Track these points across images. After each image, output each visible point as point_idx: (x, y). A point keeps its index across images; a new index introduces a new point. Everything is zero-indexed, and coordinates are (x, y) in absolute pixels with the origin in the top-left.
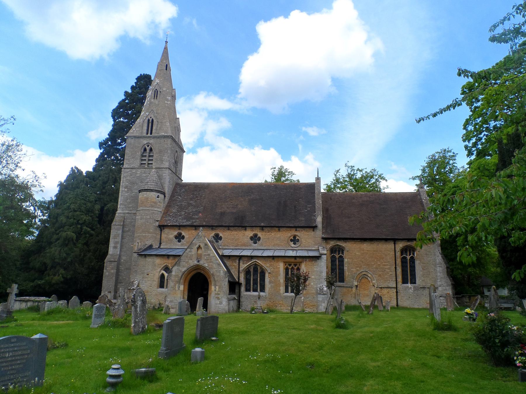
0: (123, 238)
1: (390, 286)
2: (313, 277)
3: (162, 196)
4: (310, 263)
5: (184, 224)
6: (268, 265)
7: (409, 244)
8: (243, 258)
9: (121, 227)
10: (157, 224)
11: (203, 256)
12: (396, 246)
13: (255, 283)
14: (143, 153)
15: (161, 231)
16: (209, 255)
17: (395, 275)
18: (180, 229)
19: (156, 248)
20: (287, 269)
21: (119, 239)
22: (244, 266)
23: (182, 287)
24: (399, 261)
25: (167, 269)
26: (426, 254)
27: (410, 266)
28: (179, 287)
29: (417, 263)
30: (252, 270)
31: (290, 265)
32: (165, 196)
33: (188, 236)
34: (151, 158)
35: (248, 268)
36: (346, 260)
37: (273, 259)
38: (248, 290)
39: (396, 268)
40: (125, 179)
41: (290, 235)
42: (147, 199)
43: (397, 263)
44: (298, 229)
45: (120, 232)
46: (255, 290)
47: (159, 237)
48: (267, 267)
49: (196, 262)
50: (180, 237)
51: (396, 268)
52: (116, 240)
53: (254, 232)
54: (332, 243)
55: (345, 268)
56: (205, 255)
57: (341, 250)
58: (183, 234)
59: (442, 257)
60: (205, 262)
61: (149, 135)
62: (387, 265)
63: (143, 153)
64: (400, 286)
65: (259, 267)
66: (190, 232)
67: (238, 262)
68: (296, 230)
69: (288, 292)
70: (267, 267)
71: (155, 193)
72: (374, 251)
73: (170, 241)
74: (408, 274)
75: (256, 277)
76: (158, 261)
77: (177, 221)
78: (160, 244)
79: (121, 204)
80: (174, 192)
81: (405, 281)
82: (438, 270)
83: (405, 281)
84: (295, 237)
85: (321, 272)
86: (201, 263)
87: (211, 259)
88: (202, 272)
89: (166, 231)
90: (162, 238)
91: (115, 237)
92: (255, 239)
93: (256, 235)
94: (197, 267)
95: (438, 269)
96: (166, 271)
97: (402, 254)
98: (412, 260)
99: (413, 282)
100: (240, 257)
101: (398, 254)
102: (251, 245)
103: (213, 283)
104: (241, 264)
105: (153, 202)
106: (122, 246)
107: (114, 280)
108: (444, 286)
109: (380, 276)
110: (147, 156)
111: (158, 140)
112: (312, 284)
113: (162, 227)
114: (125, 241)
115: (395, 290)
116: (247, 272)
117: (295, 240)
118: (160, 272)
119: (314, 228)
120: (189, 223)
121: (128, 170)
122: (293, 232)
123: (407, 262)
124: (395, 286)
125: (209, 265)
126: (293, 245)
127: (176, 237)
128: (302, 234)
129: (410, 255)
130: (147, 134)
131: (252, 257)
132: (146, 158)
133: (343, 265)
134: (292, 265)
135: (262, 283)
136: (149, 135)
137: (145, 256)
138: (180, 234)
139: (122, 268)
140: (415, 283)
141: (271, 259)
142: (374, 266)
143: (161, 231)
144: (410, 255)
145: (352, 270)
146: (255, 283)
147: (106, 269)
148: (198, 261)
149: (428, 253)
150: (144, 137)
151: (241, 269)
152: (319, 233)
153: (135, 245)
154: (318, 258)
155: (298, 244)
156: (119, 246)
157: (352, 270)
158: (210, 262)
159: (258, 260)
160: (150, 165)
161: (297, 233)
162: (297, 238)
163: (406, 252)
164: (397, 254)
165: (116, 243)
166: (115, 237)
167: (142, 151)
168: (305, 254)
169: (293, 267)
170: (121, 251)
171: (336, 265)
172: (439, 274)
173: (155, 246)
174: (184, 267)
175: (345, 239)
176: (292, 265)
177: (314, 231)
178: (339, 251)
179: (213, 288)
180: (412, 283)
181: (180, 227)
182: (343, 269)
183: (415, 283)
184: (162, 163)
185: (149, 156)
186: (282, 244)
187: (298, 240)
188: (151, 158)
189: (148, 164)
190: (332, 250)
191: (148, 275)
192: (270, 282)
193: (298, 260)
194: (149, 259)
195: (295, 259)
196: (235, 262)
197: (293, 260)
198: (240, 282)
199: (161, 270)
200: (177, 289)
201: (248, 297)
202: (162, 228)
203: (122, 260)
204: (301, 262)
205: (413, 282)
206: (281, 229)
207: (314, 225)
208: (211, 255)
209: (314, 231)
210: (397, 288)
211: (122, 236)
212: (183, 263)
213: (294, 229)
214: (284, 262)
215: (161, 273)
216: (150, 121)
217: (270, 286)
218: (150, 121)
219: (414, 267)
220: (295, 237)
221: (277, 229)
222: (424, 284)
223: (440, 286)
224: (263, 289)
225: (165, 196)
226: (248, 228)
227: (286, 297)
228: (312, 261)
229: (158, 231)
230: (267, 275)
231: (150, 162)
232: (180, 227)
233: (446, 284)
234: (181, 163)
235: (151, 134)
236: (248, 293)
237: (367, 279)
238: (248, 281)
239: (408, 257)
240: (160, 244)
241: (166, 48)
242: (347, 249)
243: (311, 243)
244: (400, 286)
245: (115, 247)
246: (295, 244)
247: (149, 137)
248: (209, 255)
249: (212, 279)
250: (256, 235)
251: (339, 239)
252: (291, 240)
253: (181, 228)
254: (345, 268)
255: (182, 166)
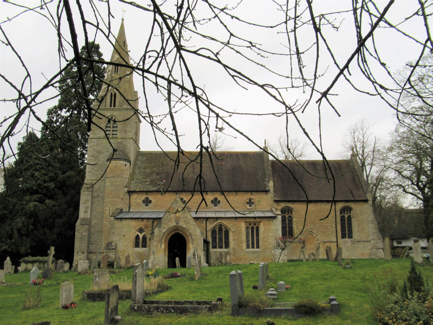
0: (92, 203)
1: (332, 240)
2: (270, 234)
3: (128, 164)
4: (267, 223)
5: (151, 189)
6: (232, 225)
7: (347, 204)
8: (210, 219)
9: (91, 193)
10: (126, 190)
11: (181, 219)
12: (336, 207)
13: (221, 240)
14: (107, 124)
15: (130, 196)
16: (186, 217)
17: (335, 231)
18: (147, 194)
19: (126, 212)
20: (247, 228)
21: (89, 204)
22: (210, 226)
23: (163, 246)
24: (339, 219)
25: (141, 230)
26: (361, 213)
27: (348, 224)
28: (161, 245)
29: (353, 220)
30: (217, 230)
31: (250, 224)
32: (130, 164)
33: (154, 201)
34: (115, 129)
35: (214, 228)
36: (294, 219)
37: (236, 219)
38: (214, 247)
39: (336, 225)
40: (91, 149)
41: (246, 198)
42: (116, 167)
43: (337, 221)
44: (253, 193)
45: (90, 198)
46: (221, 247)
47: (128, 202)
48: (231, 226)
49: (175, 224)
50: (147, 202)
51: (336, 225)
52: (86, 205)
53: (214, 196)
54: (283, 205)
55: (293, 226)
56: (183, 218)
57: (350, 209)
58: (150, 198)
59: (374, 215)
60: (183, 223)
61: (112, 107)
62: (329, 223)
63: (107, 124)
64: (340, 240)
65: (223, 227)
66: (157, 197)
67: (205, 222)
68: (251, 194)
69: (249, 248)
70: (231, 226)
71: (123, 162)
72: (318, 211)
73: (139, 204)
74: (346, 230)
75: (219, 236)
76: (133, 223)
77: (144, 187)
78: (130, 208)
79: (89, 172)
80: (136, 159)
81: (343, 236)
82: (371, 226)
83: (343, 236)
84: (250, 200)
85: (277, 230)
86: (180, 224)
87: (188, 221)
88: (180, 232)
89: (134, 196)
90: (131, 202)
91: (86, 202)
92: (147, 202)
93: (216, 199)
94: (176, 228)
95: (371, 225)
96: (140, 232)
97: (341, 213)
98: (350, 218)
99: (350, 237)
100: (207, 219)
101: (338, 213)
102: (212, 208)
103: (190, 241)
104: (208, 224)
105: (122, 170)
106: (91, 210)
107: (87, 242)
108: (375, 240)
109: (323, 232)
110: (112, 127)
111: (122, 112)
112: (270, 240)
113: (130, 193)
114: (94, 205)
115: (336, 244)
116: (214, 232)
117: (250, 202)
118: (135, 233)
119: (267, 192)
120: (154, 189)
121: (95, 140)
122: (248, 196)
123: (345, 220)
124: (335, 240)
125: (186, 226)
126: (249, 207)
127: (144, 202)
128: (256, 197)
129: (347, 214)
130: (111, 106)
131: (217, 218)
132: (111, 129)
133: (292, 224)
134: (252, 225)
135: (226, 240)
136: (112, 107)
137: (121, 219)
138: (147, 199)
139: (93, 231)
140: (352, 238)
141: (234, 220)
142: (318, 224)
143: (130, 196)
144: (347, 214)
145: (300, 227)
146: (221, 240)
147: (78, 232)
148: (177, 223)
149: (362, 212)
150: (108, 109)
151: (208, 229)
152: (270, 196)
153: (107, 210)
154: (274, 218)
155: (253, 206)
156: (89, 210)
157: (300, 227)
158: (188, 223)
159: (223, 220)
160: (114, 136)
161: (252, 197)
162: (252, 201)
163: (344, 211)
164: (337, 214)
165: (87, 208)
166: (86, 202)
167: (107, 122)
168: (262, 215)
169: (252, 227)
170: (91, 214)
171: (286, 223)
172: (371, 230)
173: (126, 209)
174: (164, 228)
175: (293, 201)
176: (252, 225)
177: (266, 194)
178: (288, 212)
179: (191, 246)
180: (349, 238)
181: (147, 192)
182: (292, 227)
183: (352, 238)
184: (126, 134)
185: (113, 127)
186: (240, 206)
187: (253, 203)
188: (115, 129)
189: (113, 134)
190: (283, 211)
191: (124, 236)
192: (234, 240)
193: (257, 220)
194: (124, 222)
195: (255, 219)
196: (203, 223)
197: (253, 220)
198: (208, 240)
199: (136, 231)
200: (159, 247)
201: (214, 252)
202: (131, 194)
203: (92, 224)
204: (260, 222)
205: (350, 237)
206: (239, 193)
207: (268, 189)
208: (188, 217)
209: (266, 194)
210: (337, 242)
211: (92, 201)
212: (163, 225)
213: (250, 193)
214: (245, 222)
215: (136, 234)
216: (113, 94)
217: (233, 243)
218: (113, 94)
219: (351, 224)
220: (250, 200)
221: (235, 193)
222: (359, 238)
223: (372, 240)
224: (227, 246)
225: (130, 164)
226: (209, 193)
227: (248, 252)
228: (269, 221)
229: (127, 196)
230: (231, 234)
231: (114, 133)
232: (147, 192)
233: (377, 238)
234: (139, 132)
235: (114, 106)
236: (215, 250)
237: (312, 235)
238: (214, 239)
239: (346, 216)
240: (130, 208)
241: (122, 26)
242: (295, 210)
243: (265, 204)
244: (340, 240)
245: (86, 212)
246: (250, 206)
247: (113, 109)
248: (186, 217)
249: (190, 238)
250: (216, 199)
251: (289, 201)
252: (247, 203)
253: (148, 193)
254: (294, 227)
255: (139, 136)
